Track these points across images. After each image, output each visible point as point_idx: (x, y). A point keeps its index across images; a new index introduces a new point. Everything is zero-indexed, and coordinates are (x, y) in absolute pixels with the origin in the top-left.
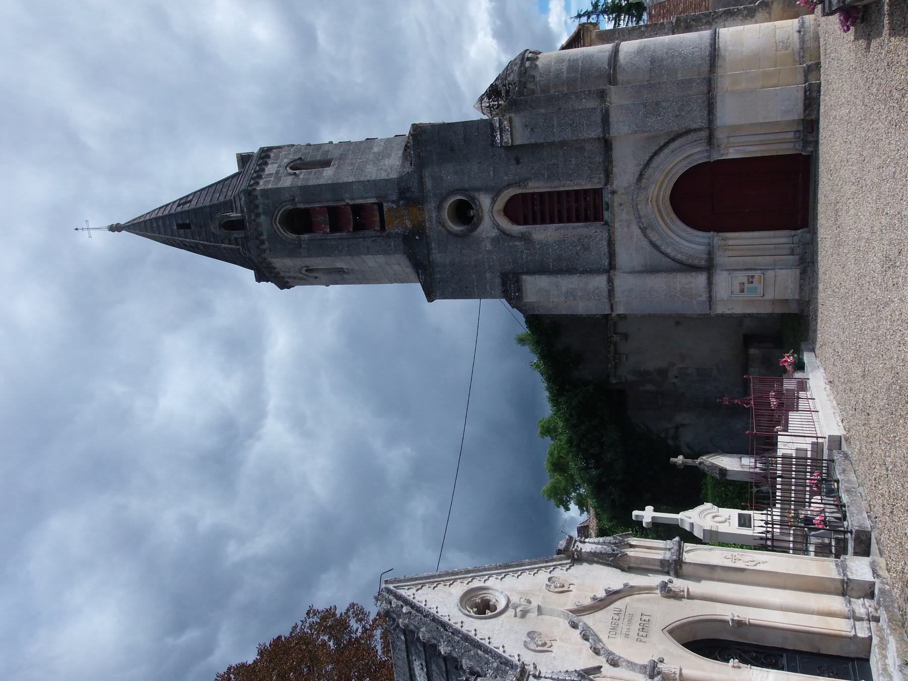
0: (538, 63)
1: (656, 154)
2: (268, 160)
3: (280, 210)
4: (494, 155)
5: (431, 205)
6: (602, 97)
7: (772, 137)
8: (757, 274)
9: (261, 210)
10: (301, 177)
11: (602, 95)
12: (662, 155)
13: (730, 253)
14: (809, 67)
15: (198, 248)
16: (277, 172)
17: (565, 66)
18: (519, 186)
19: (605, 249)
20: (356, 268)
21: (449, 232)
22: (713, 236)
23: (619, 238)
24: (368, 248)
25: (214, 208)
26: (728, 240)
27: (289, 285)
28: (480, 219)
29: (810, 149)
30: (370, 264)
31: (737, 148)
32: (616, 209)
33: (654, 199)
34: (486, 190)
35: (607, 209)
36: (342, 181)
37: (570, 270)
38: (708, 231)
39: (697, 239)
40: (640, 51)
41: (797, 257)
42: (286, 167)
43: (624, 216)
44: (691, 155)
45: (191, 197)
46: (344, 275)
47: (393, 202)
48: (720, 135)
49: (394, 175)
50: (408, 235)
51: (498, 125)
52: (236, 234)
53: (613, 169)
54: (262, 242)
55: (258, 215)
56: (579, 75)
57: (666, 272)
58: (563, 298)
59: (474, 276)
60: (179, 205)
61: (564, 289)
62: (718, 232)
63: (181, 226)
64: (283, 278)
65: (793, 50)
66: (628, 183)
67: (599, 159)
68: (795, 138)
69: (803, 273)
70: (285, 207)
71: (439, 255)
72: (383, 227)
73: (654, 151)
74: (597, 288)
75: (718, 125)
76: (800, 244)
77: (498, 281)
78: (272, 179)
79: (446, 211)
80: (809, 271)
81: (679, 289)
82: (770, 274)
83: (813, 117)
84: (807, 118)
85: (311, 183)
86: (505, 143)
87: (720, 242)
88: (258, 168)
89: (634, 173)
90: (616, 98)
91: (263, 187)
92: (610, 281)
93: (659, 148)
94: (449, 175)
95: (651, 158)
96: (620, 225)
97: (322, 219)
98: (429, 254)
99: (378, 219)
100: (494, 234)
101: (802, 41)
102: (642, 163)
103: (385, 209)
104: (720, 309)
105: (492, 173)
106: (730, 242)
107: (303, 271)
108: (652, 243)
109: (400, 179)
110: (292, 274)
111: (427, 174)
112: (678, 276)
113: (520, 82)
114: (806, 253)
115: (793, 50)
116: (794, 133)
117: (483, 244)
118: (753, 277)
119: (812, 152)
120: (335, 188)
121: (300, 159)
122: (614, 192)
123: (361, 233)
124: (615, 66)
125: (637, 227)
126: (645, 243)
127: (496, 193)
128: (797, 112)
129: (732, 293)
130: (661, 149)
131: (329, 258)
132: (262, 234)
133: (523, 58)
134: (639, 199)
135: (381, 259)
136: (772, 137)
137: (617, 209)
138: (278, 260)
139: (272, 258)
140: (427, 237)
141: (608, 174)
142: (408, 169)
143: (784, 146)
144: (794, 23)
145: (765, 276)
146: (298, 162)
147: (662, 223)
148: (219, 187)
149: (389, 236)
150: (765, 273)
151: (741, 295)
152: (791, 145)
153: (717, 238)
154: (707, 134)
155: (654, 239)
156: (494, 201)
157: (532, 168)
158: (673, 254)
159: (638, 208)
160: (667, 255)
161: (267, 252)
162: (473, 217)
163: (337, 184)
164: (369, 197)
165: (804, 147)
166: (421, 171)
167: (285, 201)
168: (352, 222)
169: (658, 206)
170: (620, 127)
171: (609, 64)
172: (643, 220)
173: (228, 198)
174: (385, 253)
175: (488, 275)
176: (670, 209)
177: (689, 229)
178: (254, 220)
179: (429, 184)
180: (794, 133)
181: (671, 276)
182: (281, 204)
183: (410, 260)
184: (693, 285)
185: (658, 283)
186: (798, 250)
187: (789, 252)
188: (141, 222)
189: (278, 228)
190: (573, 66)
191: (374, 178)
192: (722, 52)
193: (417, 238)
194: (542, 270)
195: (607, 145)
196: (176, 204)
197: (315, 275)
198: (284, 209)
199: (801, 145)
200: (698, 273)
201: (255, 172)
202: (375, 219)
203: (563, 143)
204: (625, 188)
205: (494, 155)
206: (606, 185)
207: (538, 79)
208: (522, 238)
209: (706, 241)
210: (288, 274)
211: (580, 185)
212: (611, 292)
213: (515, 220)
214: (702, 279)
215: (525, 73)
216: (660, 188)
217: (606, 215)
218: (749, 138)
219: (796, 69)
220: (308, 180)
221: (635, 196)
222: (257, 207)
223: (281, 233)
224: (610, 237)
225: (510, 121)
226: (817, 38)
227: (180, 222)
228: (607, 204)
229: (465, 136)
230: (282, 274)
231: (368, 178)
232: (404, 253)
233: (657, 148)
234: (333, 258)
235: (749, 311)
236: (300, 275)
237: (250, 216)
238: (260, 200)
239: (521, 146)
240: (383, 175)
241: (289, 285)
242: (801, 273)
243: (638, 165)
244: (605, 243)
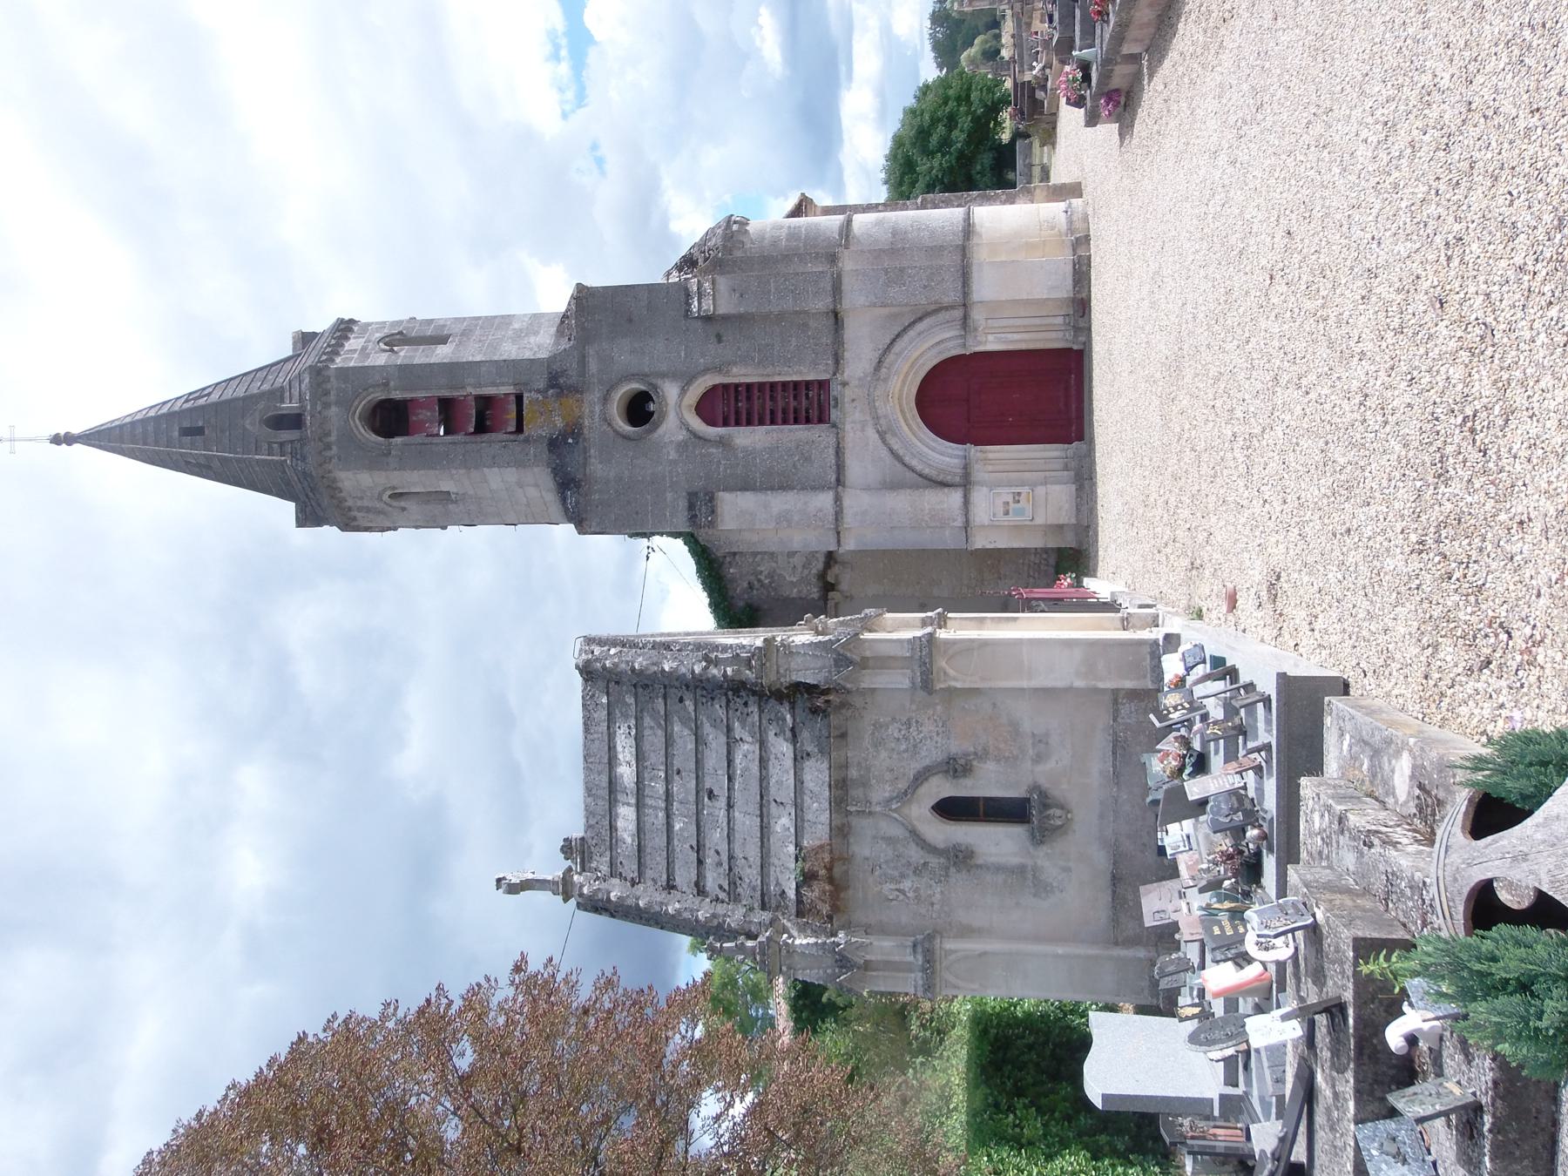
0: (747, 228)
2: (340, 349)
3: (365, 398)
4: (688, 330)
5: (594, 396)
6: (833, 261)
7: (1037, 321)
8: (1025, 490)
9: (332, 397)
10: (402, 354)
11: (833, 259)
12: (906, 338)
13: (990, 468)
14: (1077, 239)
15: (209, 467)
16: (364, 349)
17: (784, 232)
18: (720, 371)
19: (832, 459)
20: (471, 492)
21: (617, 432)
23: (850, 445)
24: (494, 457)
25: (249, 401)
27: (355, 523)
28: (663, 416)
29: (1082, 339)
30: (494, 486)
32: (847, 405)
34: (672, 375)
35: (836, 406)
36: (464, 360)
37: (784, 487)
39: (950, 451)
40: (879, 223)
41: (1072, 473)
42: (378, 342)
43: (858, 416)
44: (942, 341)
45: (210, 390)
46: (450, 506)
47: (538, 391)
48: (977, 315)
49: (544, 355)
50: (557, 437)
51: (695, 289)
52: (286, 435)
54: (328, 447)
55: (327, 406)
56: (801, 245)
57: (910, 488)
58: (774, 524)
59: (649, 497)
60: (187, 401)
63: (186, 432)
64: (350, 509)
65: (1059, 231)
67: (826, 339)
68: (1065, 324)
69: (1080, 489)
70: (373, 395)
71: (600, 466)
72: (520, 429)
73: (896, 333)
74: (821, 510)
77: (683, 504)
78: (356, 356)
79: (616, 404)
80: (1086, 486)
81: (927, 511)
82: (1040, 490)
83: (1084, 295)
85: (417, 361)
86: (705, 311)
88: (333, 342)
90: (848, 264)
91: (340, 365)
92: (838, 500)
94: (624, 354)
95: (893, 341)
97: (429, 415)
98: (585, 465)
99: (513, 415)
100: (681, 437)
101: (1070, 222)
103: (526, 401)
104: (980, 542)
105: (683, 354)
107: (385, 497)
108: (892, 453)
109: (552, 359)
110: (366, 503)
111: (591, 352)
113: (724, 246)
115: (1059, 231)
117: (665, 451)
118: (1019, 494)
119: (1084, 343)
120: (453, 369)
121: (400, 333)
122: (845, 384)
123: (486, 437)
124: (847, 236)
126: (884, 453)
127: (687, 380)
128: (1065, 290)
129: (994, 515)
130: (905, 330)
131: (432, 472)
132: (328, 434)
133: (729, 221)
134: (877, 393)
135: (511, 475)
136: (1037, 321)
137: (848, 406)
138: (349, 474)
139: (340, 470)
140: (585, 440)
141: (838, 360)
142: (565, 345)
143: (1053, 335)
144: (1062, 205)
146: (398, 337)
147: (905, 428)
148: (261, 375)
149: (527, 441)
151: (1006, 518)
152: (1060, 335)
153: (973, 450)
154: (962, 315)
155: (895, 447)
156: (683, 391)
157: (739, 349)
158: (919, 467)
161: (335, 461)
162: (652, 413)
163: (457, 363)
164: (503, 384)
165: (1075, 336)
166: (584, 347)
167: (373, 386)
168: (474, 419)
170: (855, 298)
171: (840, 234)
172: (882, 421)
173: (277, 385)
174: (520, 464)
175: (669, 496)
176: (915, 411)
178: (320, 412)
179: (593, 366)
181: (917, 493)
182: (366, 389)
183: (555, 475)
184: (945, 506)
185: (900, 502)
186: (1073, 464)
188: (116, 427)
189: (356, 427)
190: (793, 235)
191: (513, 357)
192: (978, 228)
193: (570, 441)
194: (746, 486)
195: (836, 318)
196: (183, 400)
197: (403, 504)
198: (369, 398)
201: (329, 346)
202: (509, 417)
203: (781, 316)
204: (860, 379)
205: (688, 330)
206: (835, 374)
207: (748, 246)
208: (720, 442)
209: (961, 453)
210: (359, 503)
211: (801, 373)
212: (838, 514)
213: (711, 422)
214: (956, 497)
215: (732, 237)
216: (904, 382)
218: (1011, 322)
219: (1063, 241)
220: (411, 357)
221: (871, 390)
222: (327, 393)
223: (360, 432)
224: (839, 443)
225: (713, 283)
226: (1086, 219)
227: (186, 424)
228: (836, 399)
229: (650, 302)
230: (350, 503)
231: (504, 357)
232: (548, 465)
233: (900, 329)
234: (437, 472)
235: (1016, 545)
236: (379, 505)
237: (313, 405)
238: (333, 384)
239: (726, 318)
240: (528, 355)
241: (355, 523)
244: (832, 451)
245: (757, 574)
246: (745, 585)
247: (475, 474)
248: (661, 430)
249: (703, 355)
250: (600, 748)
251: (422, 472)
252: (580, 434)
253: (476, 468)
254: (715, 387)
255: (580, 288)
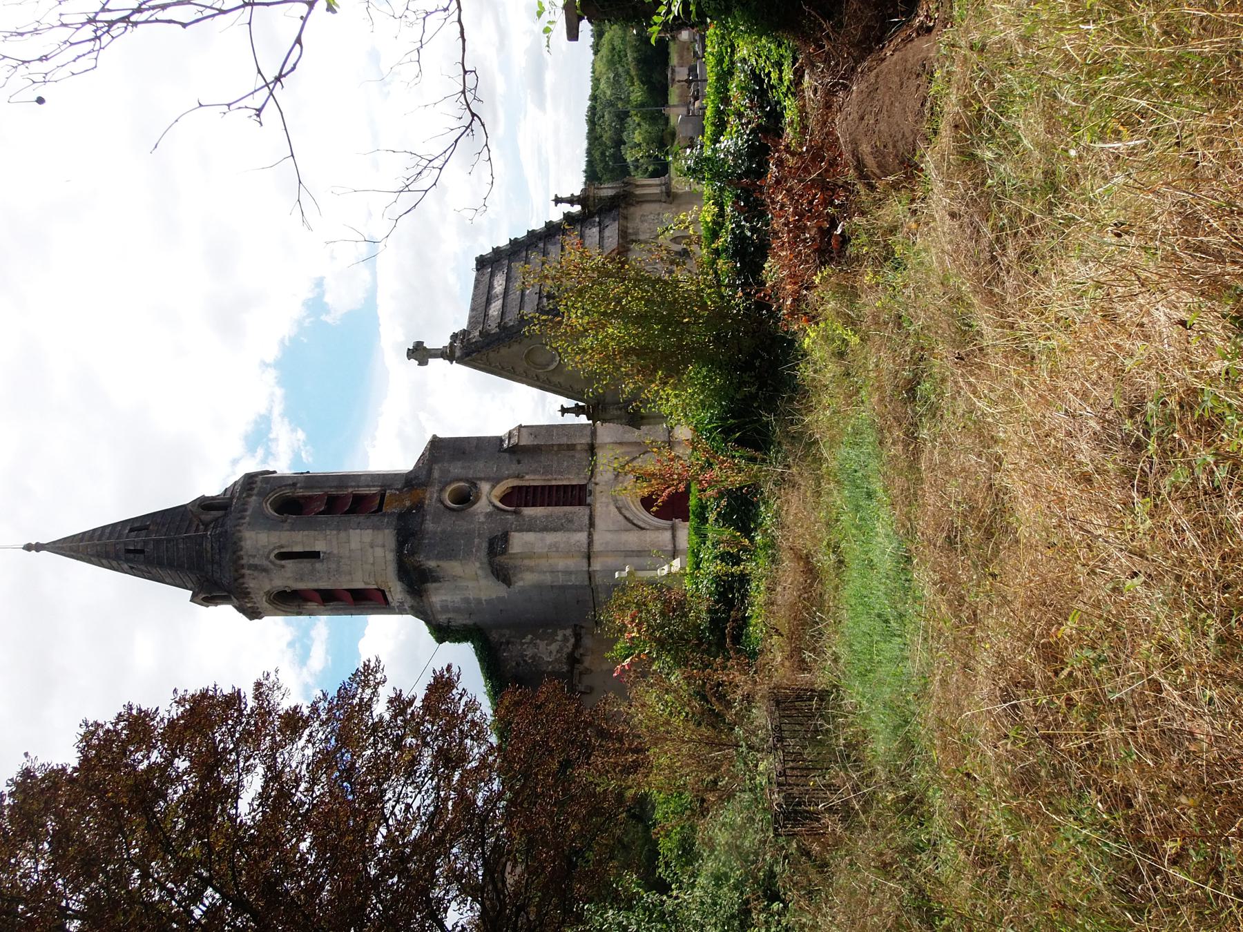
9: (255, 491)
18: (518, 477)
20: (335, 552)
21: (447, 507)
34: (487, 479)
37: (555, 530)
47: (397, 489)
61: (548, 542)
77: (485, 545)
92: (590, 535)
94: (456, 469)
110: (256, 561)
122: (596, 484)
126: (621, 518)
127: (495, 481)
131: (312, 533)
132: (245, 510)
135: (368, 535)
137: (598, 494)
149: (384, 515)
167: (285, 486)
174: (376, 528)
175: (476, 541)
212: (590, 543)
217: (589, 500)
222: (252, 489)
228: (590, 491)
230: (244, 562)
236: (265, 563)
244: (587, 517)
245: (523, 656)
246: (514, 664)
247: (343, 534)
248: (476, 506)
249: (508, 470)
250: (484, 288)
251: (306, 533)
252: (422, 507)
253: (345, 530)
254: (513, 487)
255: (435, 437)
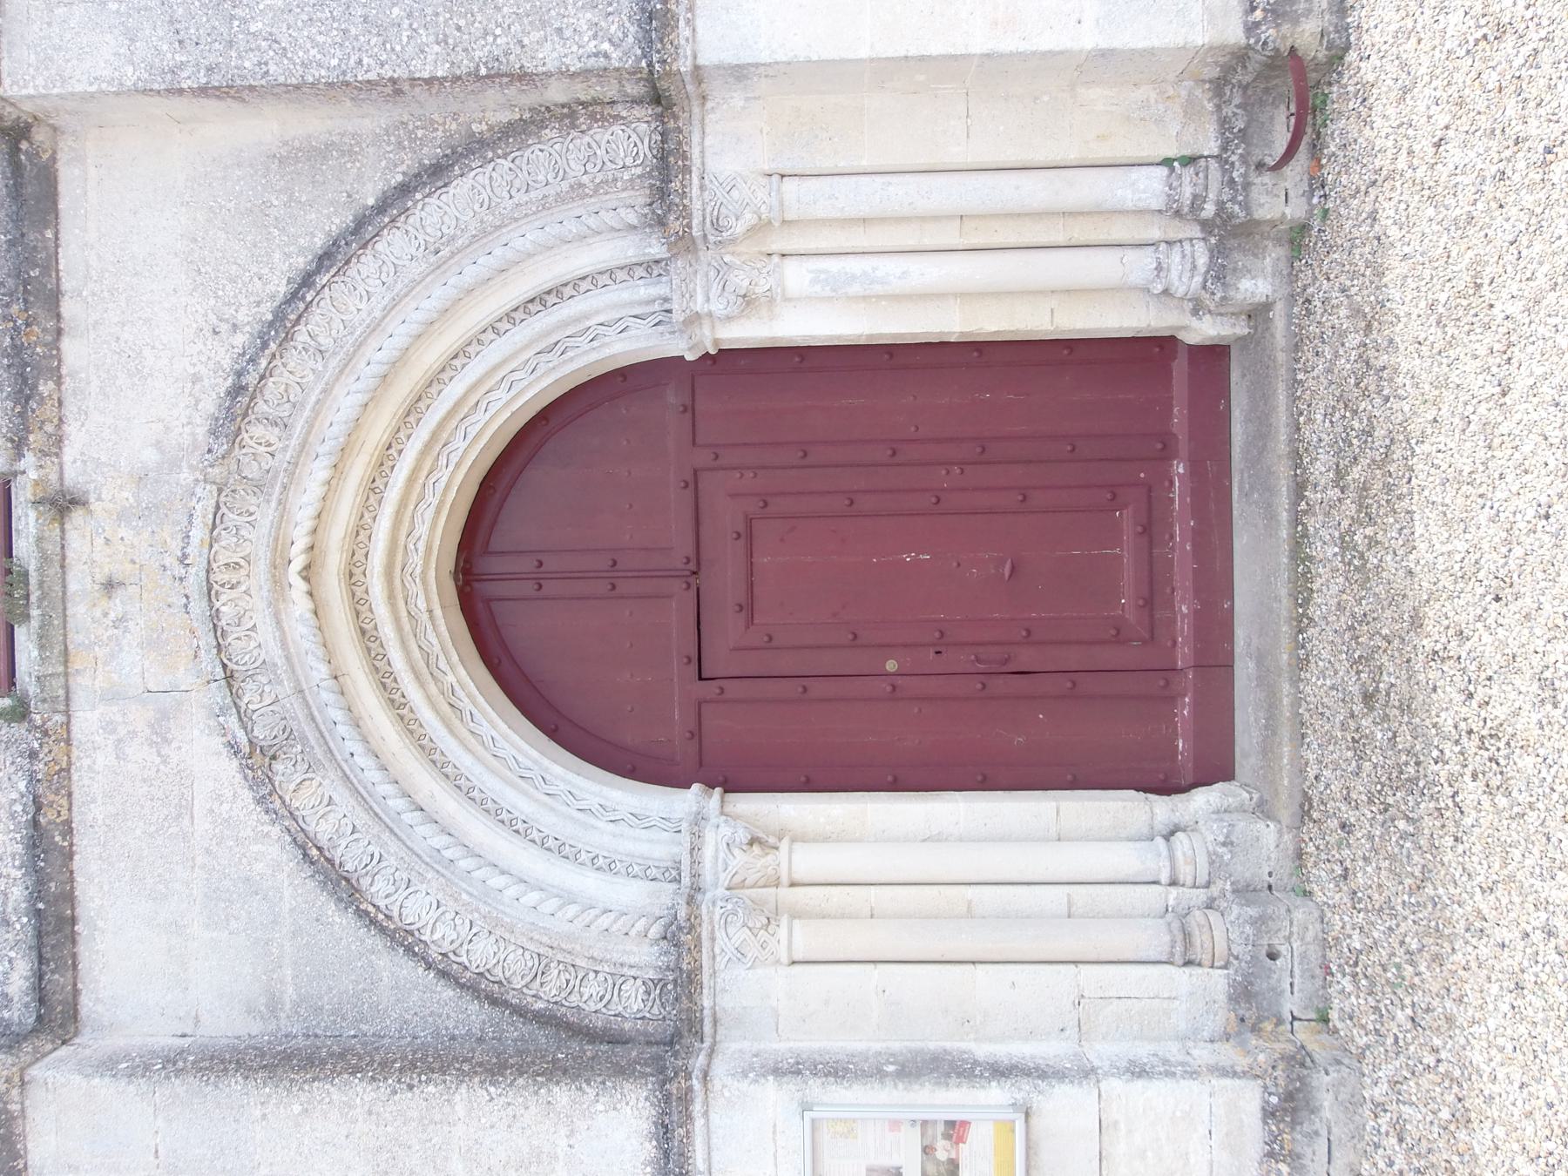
1: (329, 258)
13: (806, 939)
22: (699, 819)
26: (784, 845)
31: (833, 265)
32: (78, 611)
33: (334, 562)
38: (679, 781)
39: (602, 838)
41: (1217, 982)
53: (66, 344)
62: (731, 787)
66: (158, 445)
73: (319, 242)
75: (708, 57)
76: (1222, 885)
80: (1326, 1101)
84: (1268, 32)
87: (739, 859)
89: (196, 379)
93: (349, 219)
96: (109, 727)
102: (242, 317)
106: (806, 861)
112: (460, 1109)
114: (1272, 956)
116: (796, 922)
118: (956, 1130)
125: (217, 742)
136: (1034, 191)
145: (1034, 1121)
150: (1037, 1101)
155: (323, 830)
158: (441, 935)
159: (215, 616)
160: (404, 941)
169: (358, 604)
177: (558, 770)
180: (1164, 171)
187: (1154, 938)
199: (1202, 260)
200: (591, 1092)
209: (661, 848)
242: (1269, 1114)
243: (224, 328)
